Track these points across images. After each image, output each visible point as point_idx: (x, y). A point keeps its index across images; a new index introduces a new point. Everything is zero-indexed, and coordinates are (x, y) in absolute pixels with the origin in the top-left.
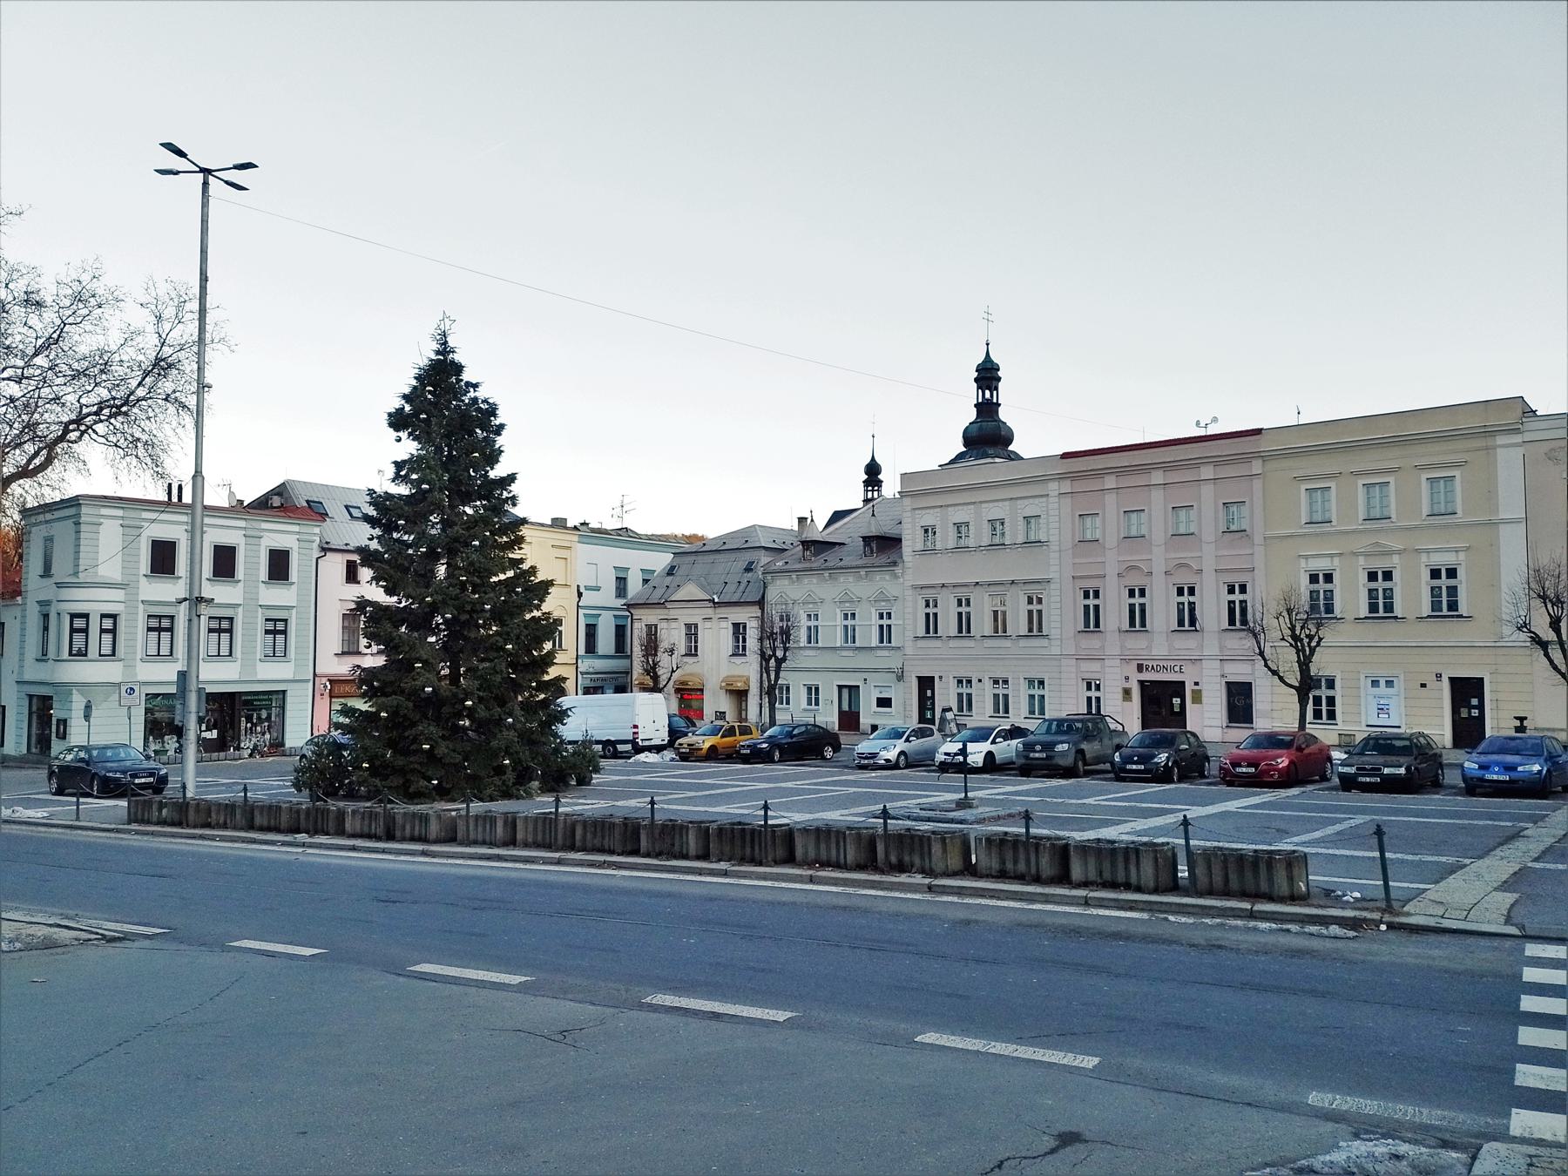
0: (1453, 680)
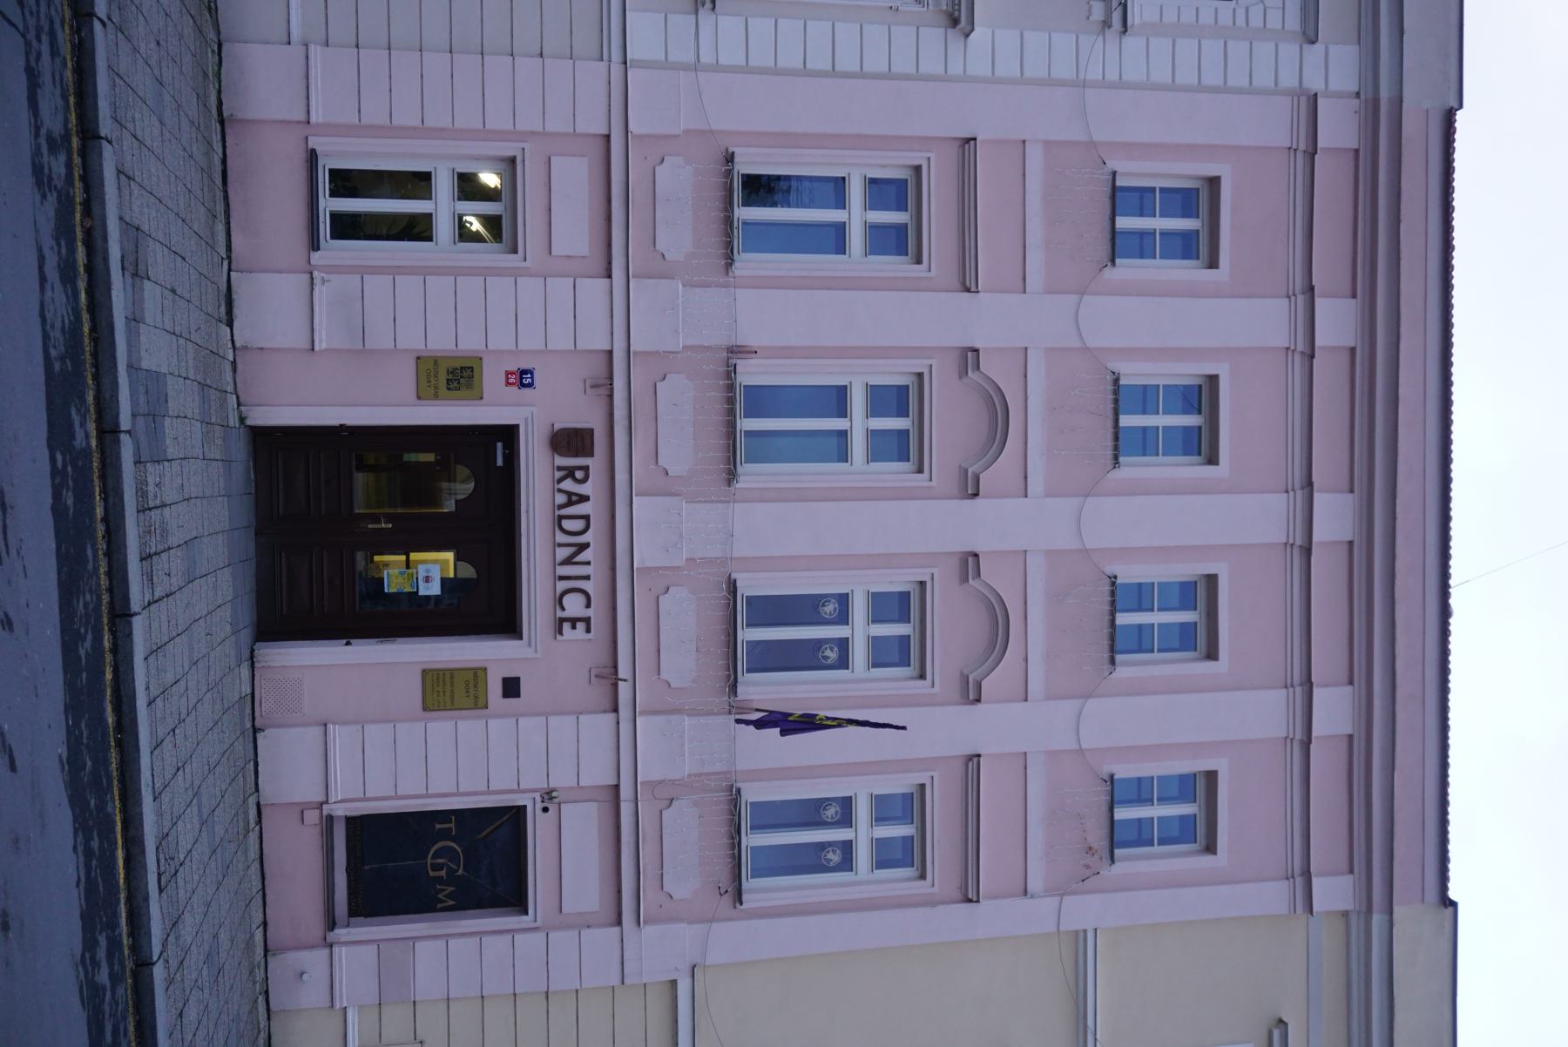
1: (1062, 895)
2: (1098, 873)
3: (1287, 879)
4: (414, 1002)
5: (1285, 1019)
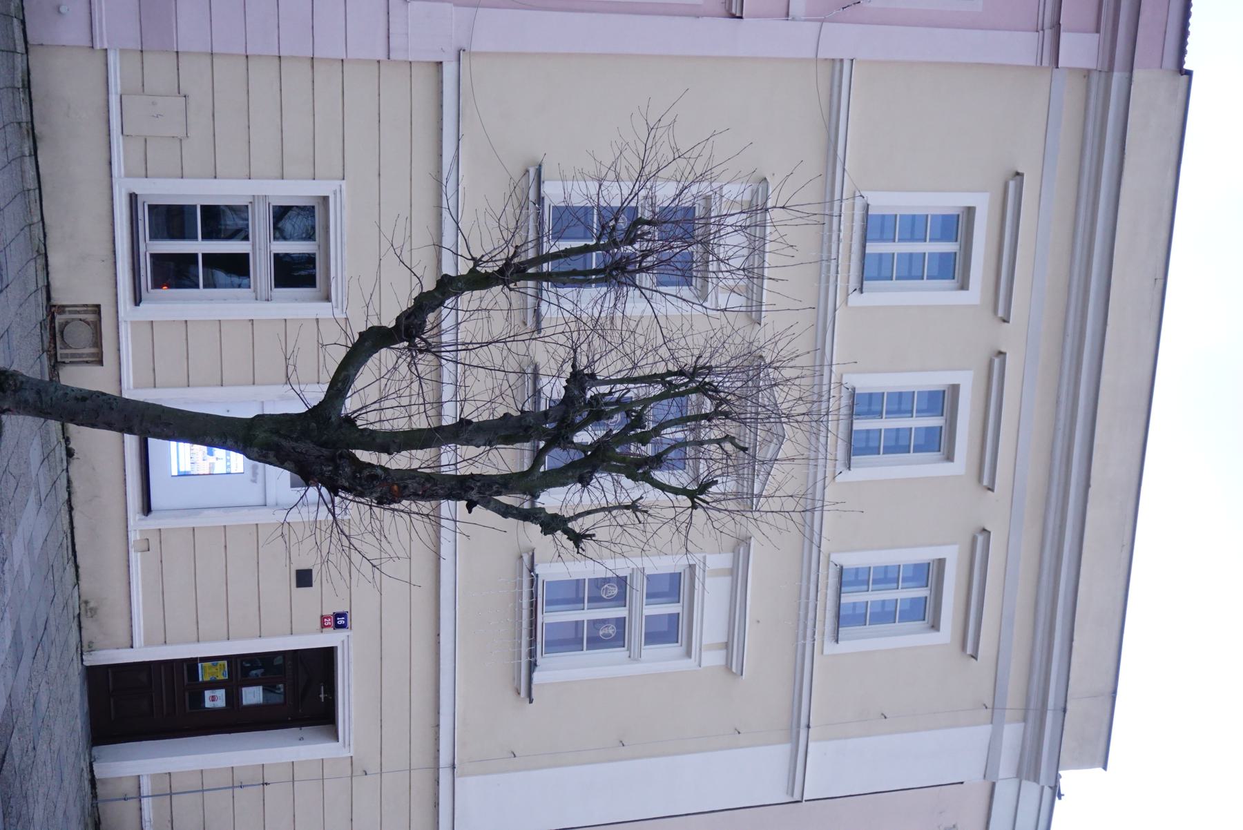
0: (328, 655)
1: (822, 21)
2: (859, 2)
3: (1037, 31)
4: (177, 52)
5: (1020, 171)
